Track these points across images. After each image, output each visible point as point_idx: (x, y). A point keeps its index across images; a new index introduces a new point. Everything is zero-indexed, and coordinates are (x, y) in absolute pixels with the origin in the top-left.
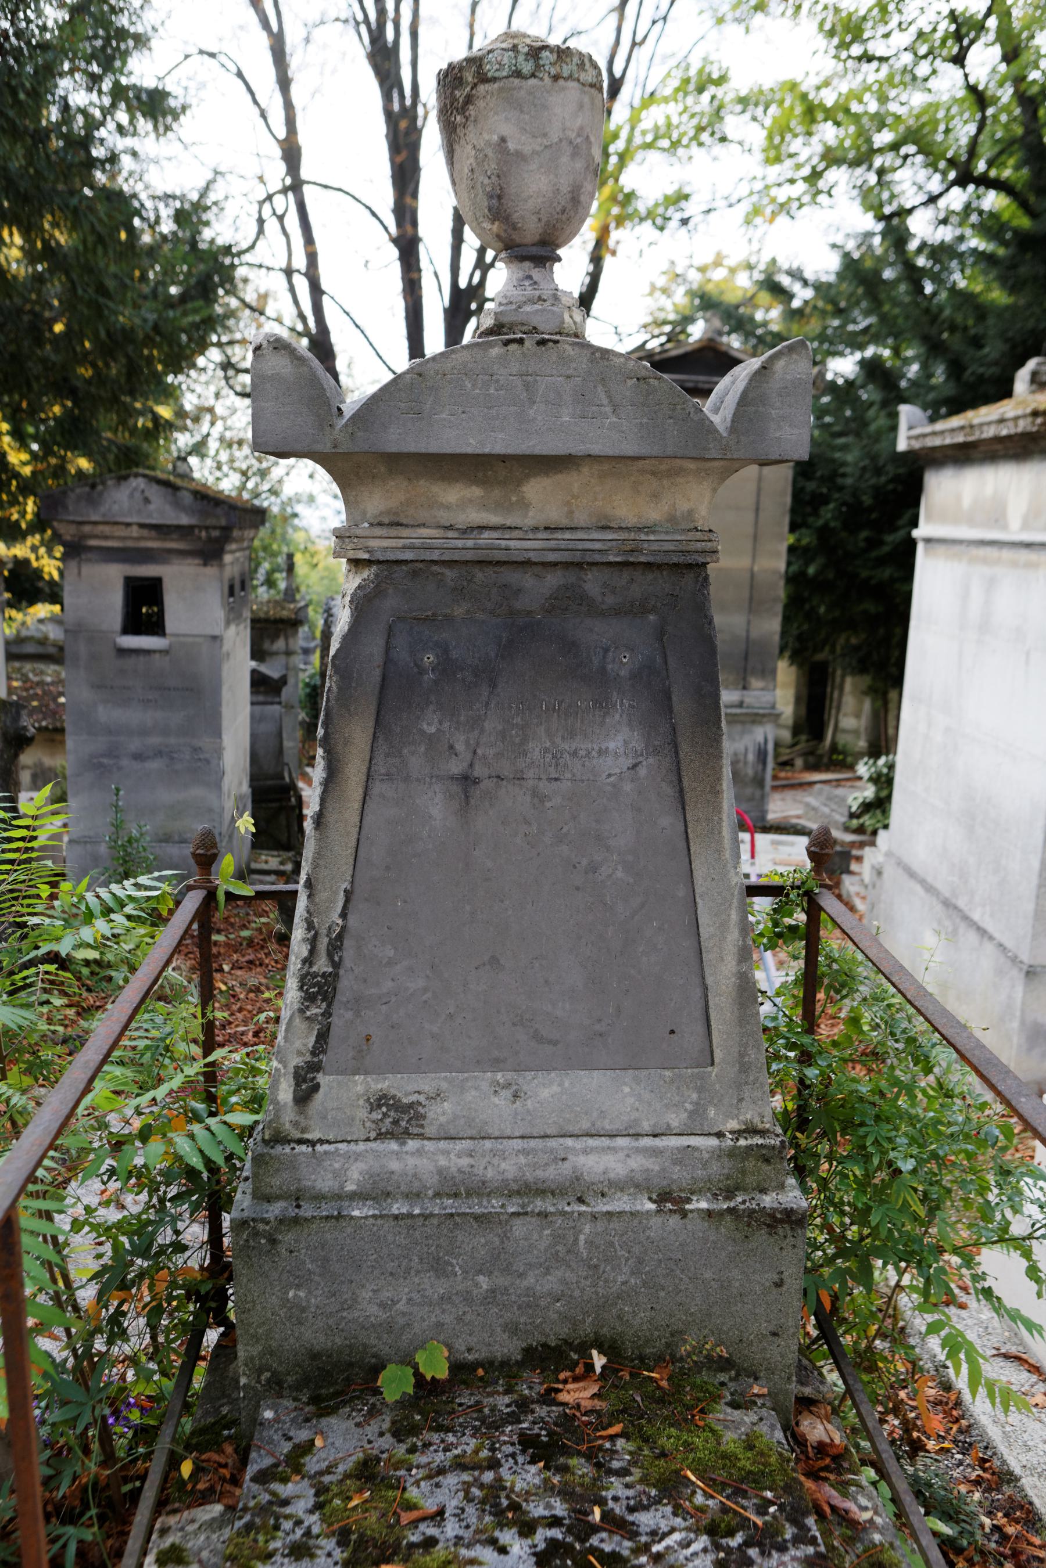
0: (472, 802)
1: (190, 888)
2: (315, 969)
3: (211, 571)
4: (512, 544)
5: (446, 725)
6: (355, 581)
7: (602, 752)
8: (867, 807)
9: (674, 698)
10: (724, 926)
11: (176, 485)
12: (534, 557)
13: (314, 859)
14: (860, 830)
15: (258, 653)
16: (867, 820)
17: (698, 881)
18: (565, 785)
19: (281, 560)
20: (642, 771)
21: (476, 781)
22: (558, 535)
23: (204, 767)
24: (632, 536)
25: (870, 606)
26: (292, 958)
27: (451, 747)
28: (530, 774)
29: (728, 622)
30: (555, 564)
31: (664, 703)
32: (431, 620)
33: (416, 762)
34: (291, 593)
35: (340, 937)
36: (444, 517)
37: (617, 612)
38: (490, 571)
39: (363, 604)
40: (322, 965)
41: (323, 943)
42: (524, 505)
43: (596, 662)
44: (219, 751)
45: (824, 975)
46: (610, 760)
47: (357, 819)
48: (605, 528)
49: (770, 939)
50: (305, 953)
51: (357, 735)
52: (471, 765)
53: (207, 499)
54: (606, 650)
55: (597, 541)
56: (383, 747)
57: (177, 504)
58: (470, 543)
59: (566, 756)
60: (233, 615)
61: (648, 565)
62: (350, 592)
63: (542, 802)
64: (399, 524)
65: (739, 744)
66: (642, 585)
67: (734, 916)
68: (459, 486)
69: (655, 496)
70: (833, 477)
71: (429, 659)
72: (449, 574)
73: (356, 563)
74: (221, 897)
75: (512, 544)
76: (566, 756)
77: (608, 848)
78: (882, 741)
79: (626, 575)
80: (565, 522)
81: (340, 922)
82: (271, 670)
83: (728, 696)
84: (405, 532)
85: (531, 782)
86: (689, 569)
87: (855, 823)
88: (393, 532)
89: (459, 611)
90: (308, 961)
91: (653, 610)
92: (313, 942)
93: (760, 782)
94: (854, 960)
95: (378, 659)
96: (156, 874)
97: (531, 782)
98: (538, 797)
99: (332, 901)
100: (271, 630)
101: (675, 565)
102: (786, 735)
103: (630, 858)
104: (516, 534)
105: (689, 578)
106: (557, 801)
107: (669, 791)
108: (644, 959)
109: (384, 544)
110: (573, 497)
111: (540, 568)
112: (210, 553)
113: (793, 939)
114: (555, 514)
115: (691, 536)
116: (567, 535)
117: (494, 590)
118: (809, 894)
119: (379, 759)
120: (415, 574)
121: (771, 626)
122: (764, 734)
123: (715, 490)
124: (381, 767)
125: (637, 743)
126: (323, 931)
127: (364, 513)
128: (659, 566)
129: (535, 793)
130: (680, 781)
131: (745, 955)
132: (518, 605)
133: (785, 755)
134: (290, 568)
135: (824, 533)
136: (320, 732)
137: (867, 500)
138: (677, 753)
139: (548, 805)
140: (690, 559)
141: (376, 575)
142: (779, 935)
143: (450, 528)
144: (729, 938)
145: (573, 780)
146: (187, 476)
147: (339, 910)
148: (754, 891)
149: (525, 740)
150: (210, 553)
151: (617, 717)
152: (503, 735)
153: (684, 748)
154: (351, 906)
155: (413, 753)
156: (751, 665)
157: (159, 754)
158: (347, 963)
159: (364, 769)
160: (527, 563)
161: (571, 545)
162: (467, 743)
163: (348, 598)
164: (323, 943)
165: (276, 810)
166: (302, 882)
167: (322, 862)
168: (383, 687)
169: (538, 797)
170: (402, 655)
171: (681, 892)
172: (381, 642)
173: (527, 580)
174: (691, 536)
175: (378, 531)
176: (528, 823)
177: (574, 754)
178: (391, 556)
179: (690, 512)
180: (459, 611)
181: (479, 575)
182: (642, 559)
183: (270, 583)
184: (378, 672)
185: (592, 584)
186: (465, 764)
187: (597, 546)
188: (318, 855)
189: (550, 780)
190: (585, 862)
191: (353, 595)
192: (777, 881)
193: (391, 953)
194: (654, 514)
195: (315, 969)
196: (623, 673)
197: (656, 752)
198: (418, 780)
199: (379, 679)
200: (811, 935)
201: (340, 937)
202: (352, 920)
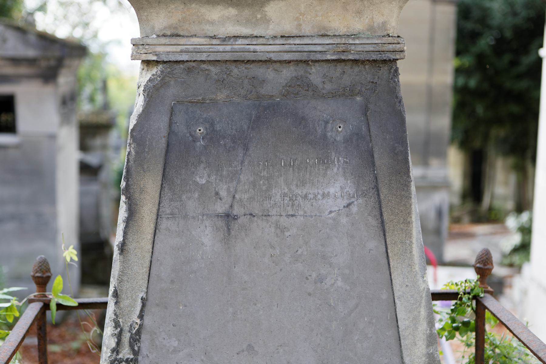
0: (233, 233)
1: (31, 301)
2: (120, 356)
3: (48, 90)
4: (258, 48)
5: (213, 178)
6: (148, 76)
7: (324, 196)
8: (516, 250)
9: (376, 156)
10: (416, 320)
11: (24, 30)
12: (274, 57)
13: (120, 276)
14: (511, 265)
15: (83, 147)
16: (516, 259)
17: (396, 287)
18: (299, 220)
19: (99, 85)
20: (354, 209)
21: (235, 218)
22: (291, 41)
23: (45, 228)
24: (343, 41)
25: (515, 109)
26: (104, 348)
27: (217, 194)
28: (273, 212)
29: (415, 120)
30: (289, 62)
31: (369, 160)
32: (202, 102)
33: (192, 205)
34: (106, 106)
35: (139, 332)
36: (210, 30)
37: (334, 95)
38: (242, 67)
39: (152, 93)
40: (126, 353)
41: (126, 337)
42: (266, 20)
43: (319, 131)
44: (54, 216)
45: (489, 357)
46: (330, 201)
47: (151, 246)
48: (323, 36)
49: (450, 332)
50: (113, 345)
51: (150, 186)
52: (231, 206)
53: (47, 40)
54: (327, 122)
55: (318, 45)
56: (168, 194)
57: (26, 43)
58: (228, 48)
59: (299, 198)
60: (65, 119)
61: (355, 61)
62: (143, 84)
63: (282, 232)
64: (178, 36)
65: (422, 206)
66: (351, 76)
67: (423, 312)
68: (220, 8)
69: (359, 13)
70: (484, 19)
71: (200, 130)
72: (214, 70)
73: (147, 63)
74: (53, 306)
75: (258, 48)
76: (299, 198)
77: (331, 265)
78: (523, 204)
79: (340, 68)
80: (295, 32)
81: (138, 321)
82: (93, 159)
83: (415, 172)
84: (182, 41)
85: (274, 218)
86: (384, 63)
87: (507, 261)
88: (174, 41)
89: (221, 96)
90: (116, 350)
91: (359, 93)
92: (119, 337)
93: (438, 232)
94: (510, 346)
95: (164, 132)
96: (6, 290)
97: (274, 218)
98: (281, 229)
99: (133, 306)
100: (92, 131)
101: (375, 61)
102: (456, 200)
103: (347, 271)
104: (260, 41)
105: (384, 69)
106: (294, 231)
107: (374, 222)
108: (359, 345)
109: (167, 50)
110: (301, 14)
111: (278, 65)
112: (49, 76)
113: (466, 332)
114: (288, 27)
115: (385, 40)
116: (297, 41)
117: (246, 81)
118: (476, 297)
119: (165, 203)
120: (189, 70)
121: (443, 122)
122: (442, 199)
123: (401, 8)
124: (166, 209)
125: (350, 188)
126: (126, 328)
127: (153, 28)
128: (363, 62)
129: (277, 226)
130: (381, 215)
131: (432, 340)
132: (263, 91)
133: (456, 214)
134: (105, 88)
135: (481, 58)
136: (123, 184)
137: (508, 34)
138: (379, 195)
139: (287, 234)
140: (385, 57)
141: (162, 72)
142: (457, 329)
143: (214, 37)
144: (420, 329)
145: (305, 216)
146: (33, 24)
147: (138, 313)
148: (437, 296)
149: (269, 189)
150: (49, 76)
151: (335, 170)
152: (254, 184)
153: (384, 191)
154: (146, 309)
155: (189, 198)
156: (430, 150)
157: (13, 217)
158: (144, 351)
159: (155, 210)
160: (268, 62)
161: (300, 48)
162: (228, 190)
163: (142, 88)
164: (126, 337)
165: (95, 259)
166: (111, 292)
167: (125, 278)
168: (167, 152)
169: (281, 229)
170: (181, 128)
171: (384, 296)
172: (166, 119)
173: (269, 73)
174: (385, 40)
175: (163, 40)
176: (272, 247)
177: (305, 197)
178: (172, 58)
179: (384, 24)
180: (221, 96)
181: (235, 71)
182: (351, 57)
183: (92, 99)
184: (163, 141)
185: (315, 75)
186: (227, 206)
187: (319, 48)
188: (122, 273)
189: (288, 216)
190: (314, 275)
191: (146, 86)
192: (453, 289)
193: (176, 344)
194: (358, 25)
195: (120, 356)
196: (338, 139)
197: (364, 195)
198: (193, 218)
199: (165, 146)
200: (479, 329)
201: (139, 332)
202: (147, 320)
